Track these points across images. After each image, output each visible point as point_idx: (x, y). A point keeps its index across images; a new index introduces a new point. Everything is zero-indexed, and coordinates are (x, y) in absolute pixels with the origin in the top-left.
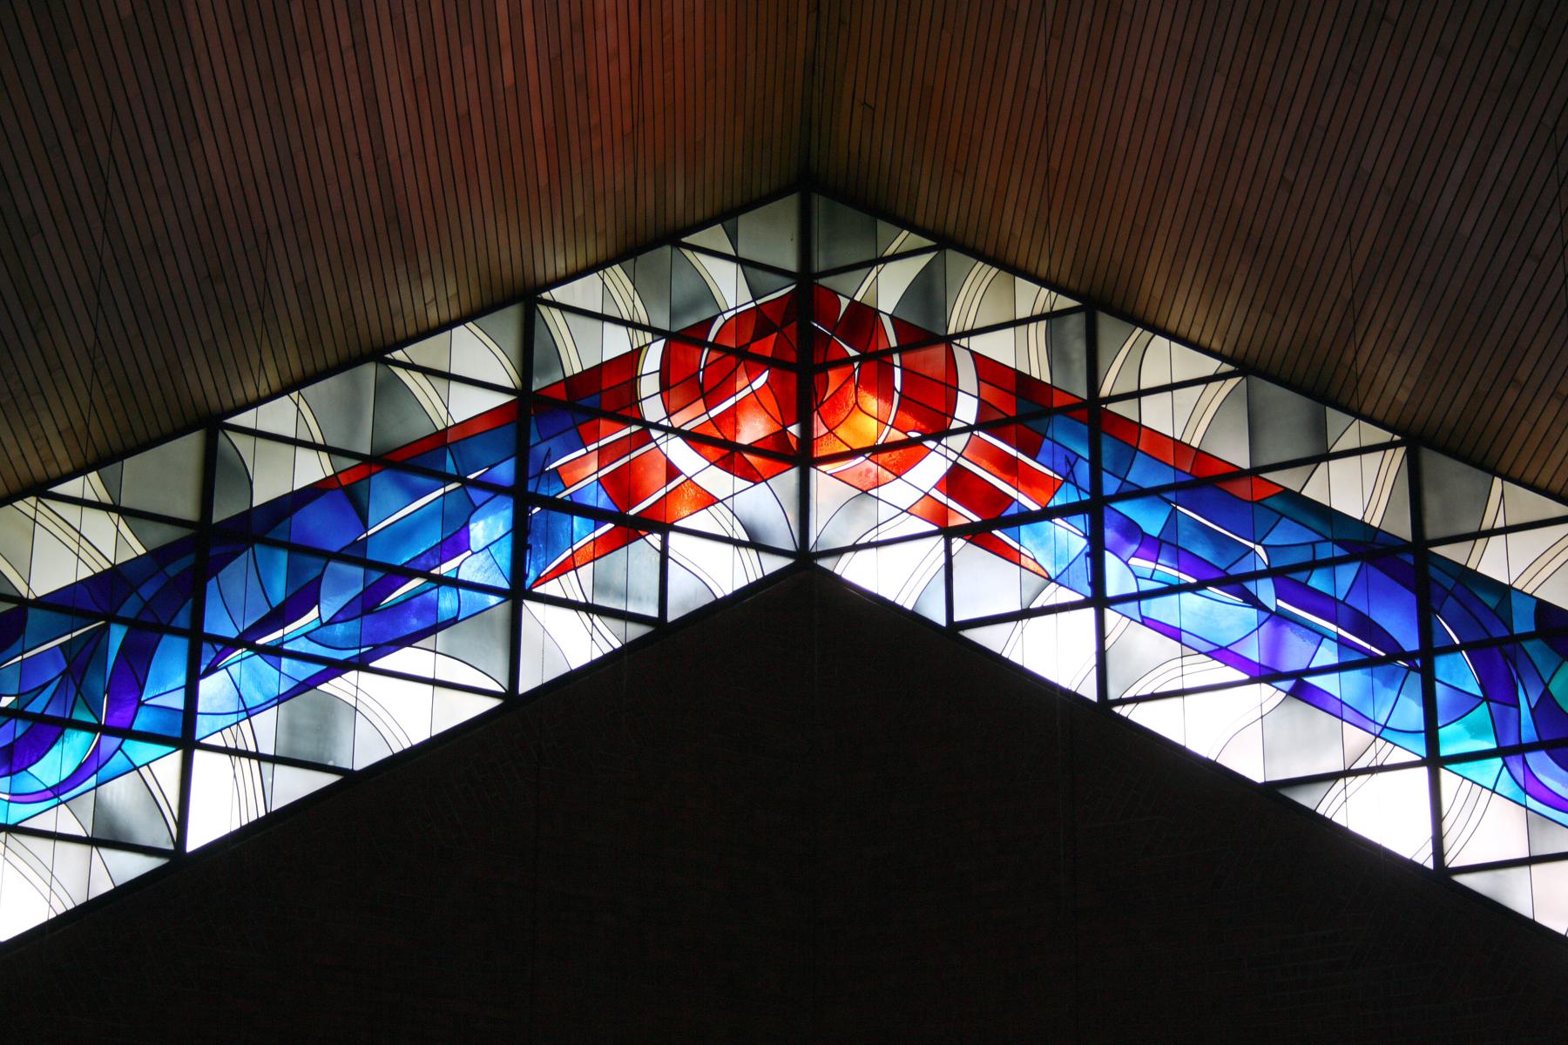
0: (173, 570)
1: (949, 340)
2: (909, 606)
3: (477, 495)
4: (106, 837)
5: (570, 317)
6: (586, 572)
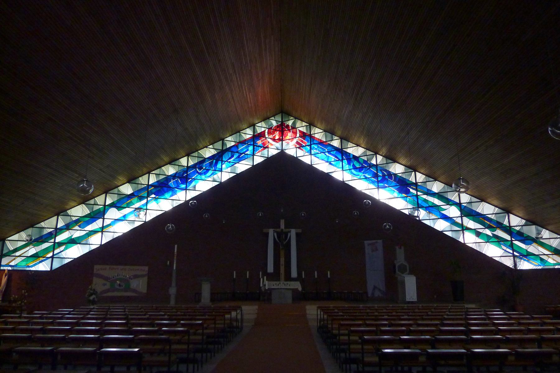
0: (220, 154)
1: (296, 128)
2: (292, 155)
3: (249, 145)
4: (214, 181)
5: (258, 127)
6: (260, 153)
